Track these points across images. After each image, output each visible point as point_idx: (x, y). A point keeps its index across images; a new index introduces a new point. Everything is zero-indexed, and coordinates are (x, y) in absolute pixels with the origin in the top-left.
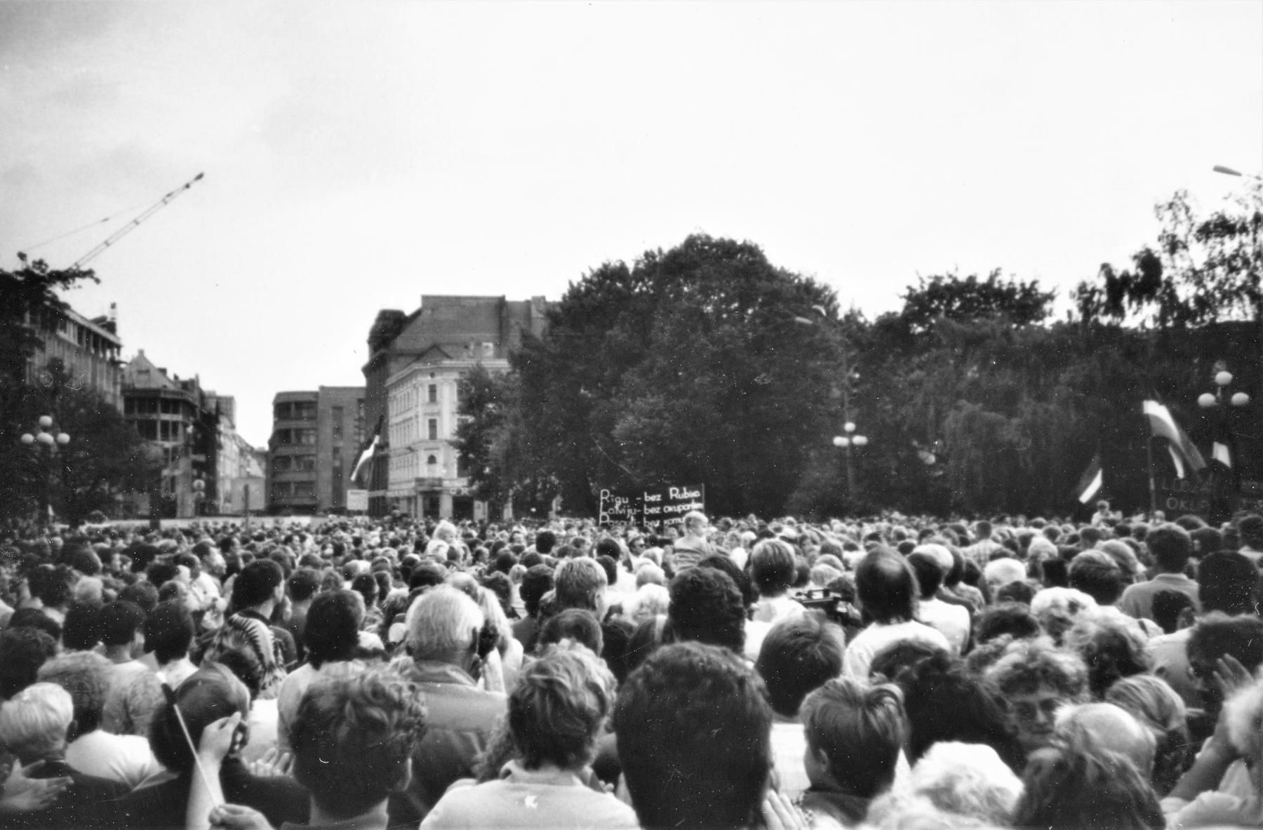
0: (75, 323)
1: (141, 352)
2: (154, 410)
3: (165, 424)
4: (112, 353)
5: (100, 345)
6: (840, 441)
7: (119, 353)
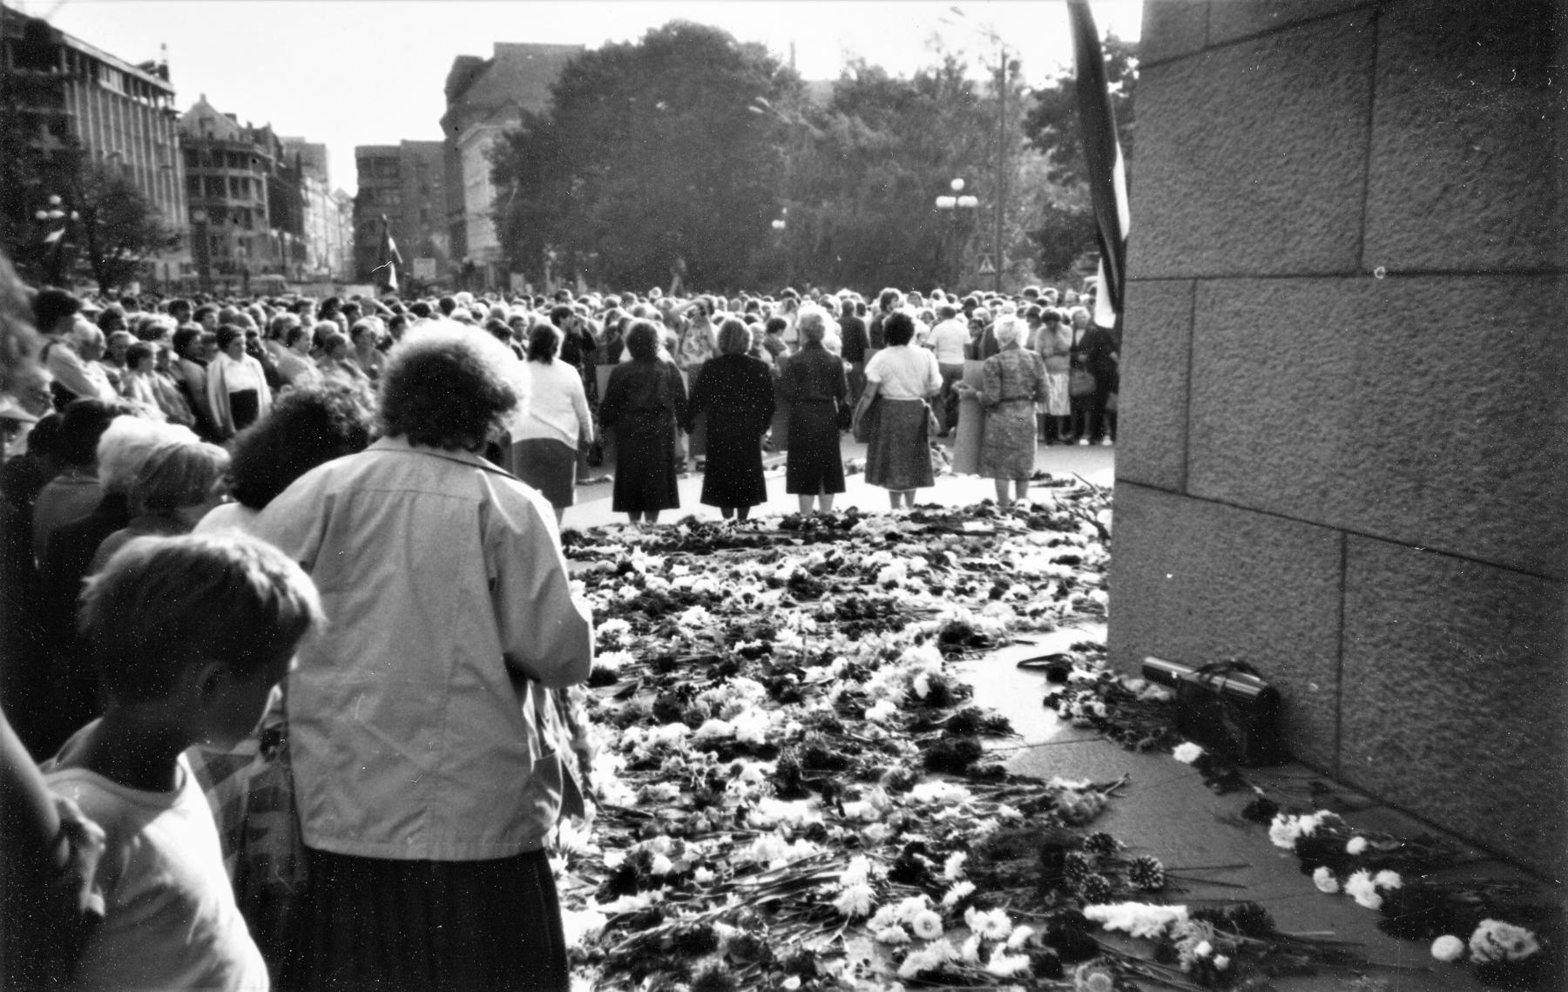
0: (118, 70)
1: (203, 97)
2: (220, 165)
3: (234, 181)
4: (166, 100)
5: (150, 92)
6: (944, 201)
7: (172, 100)
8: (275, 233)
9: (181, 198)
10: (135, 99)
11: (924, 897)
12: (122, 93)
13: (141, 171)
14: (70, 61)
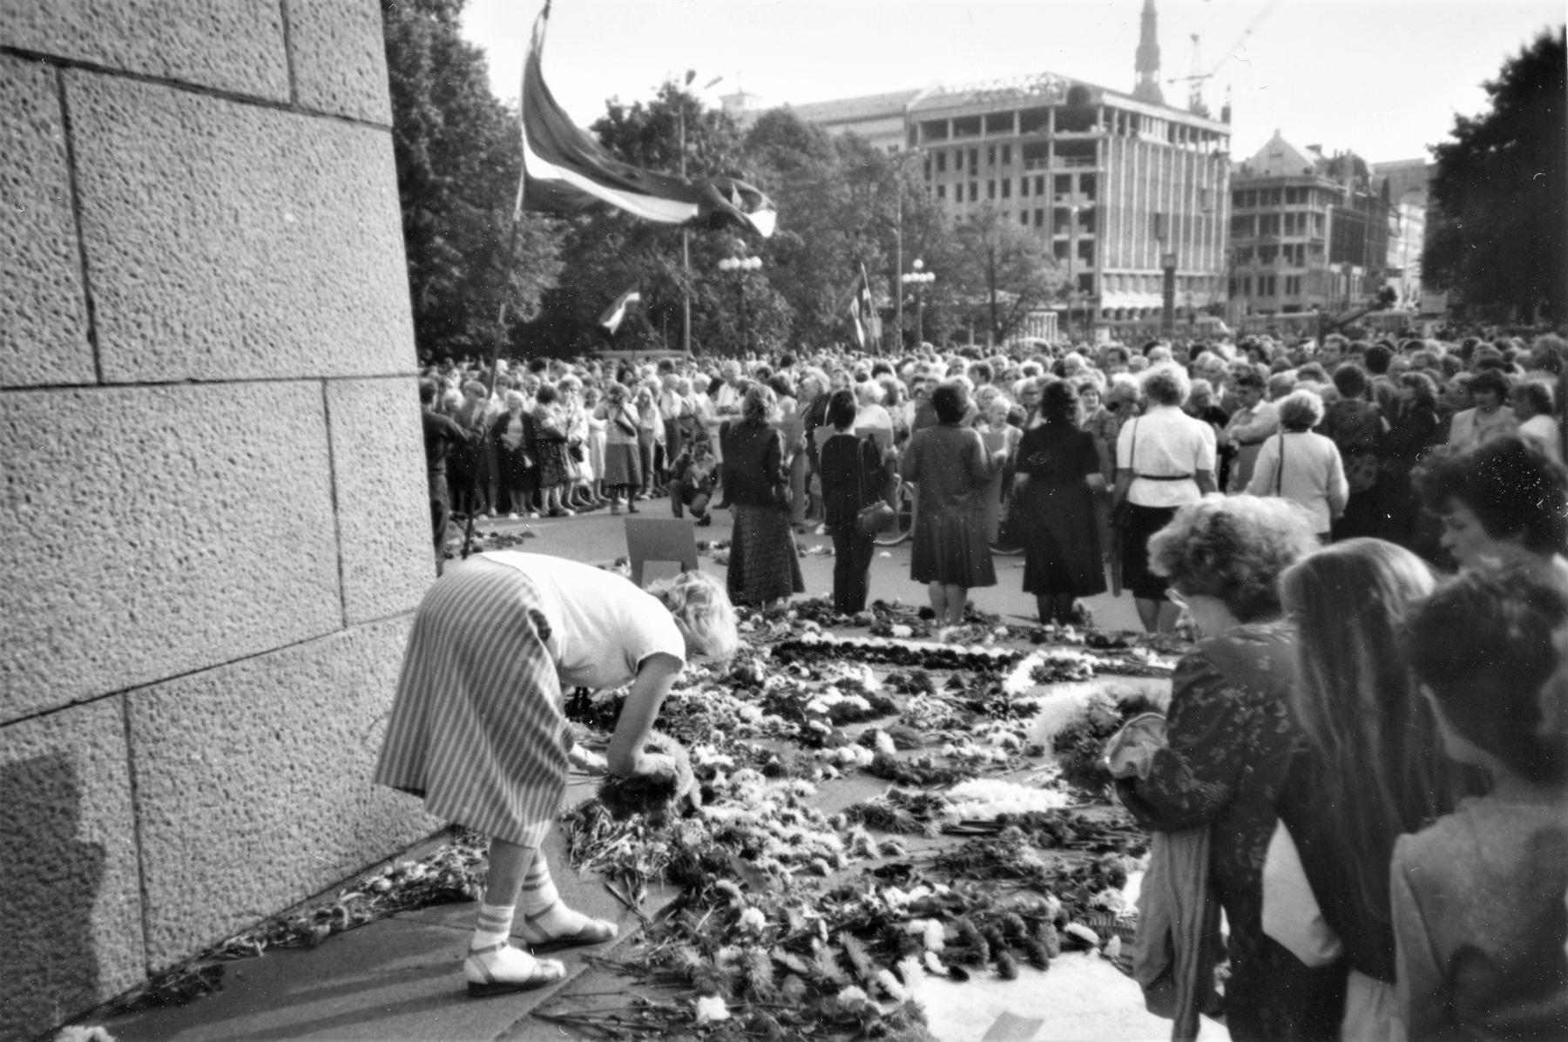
1: (1277, 133)
3: (1289, 217)
8: (1336, 268)
9: (1223, 240)
10: (1181, 147)
11: (504, 436)
12: (1166, 142)
13: (1176, 218)
14: (1108, 120)
